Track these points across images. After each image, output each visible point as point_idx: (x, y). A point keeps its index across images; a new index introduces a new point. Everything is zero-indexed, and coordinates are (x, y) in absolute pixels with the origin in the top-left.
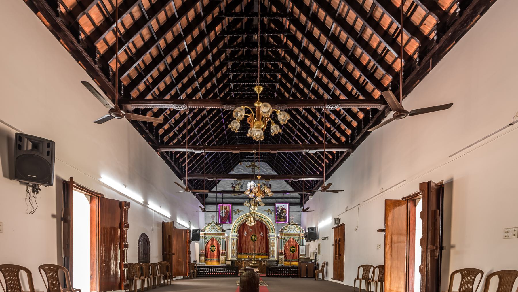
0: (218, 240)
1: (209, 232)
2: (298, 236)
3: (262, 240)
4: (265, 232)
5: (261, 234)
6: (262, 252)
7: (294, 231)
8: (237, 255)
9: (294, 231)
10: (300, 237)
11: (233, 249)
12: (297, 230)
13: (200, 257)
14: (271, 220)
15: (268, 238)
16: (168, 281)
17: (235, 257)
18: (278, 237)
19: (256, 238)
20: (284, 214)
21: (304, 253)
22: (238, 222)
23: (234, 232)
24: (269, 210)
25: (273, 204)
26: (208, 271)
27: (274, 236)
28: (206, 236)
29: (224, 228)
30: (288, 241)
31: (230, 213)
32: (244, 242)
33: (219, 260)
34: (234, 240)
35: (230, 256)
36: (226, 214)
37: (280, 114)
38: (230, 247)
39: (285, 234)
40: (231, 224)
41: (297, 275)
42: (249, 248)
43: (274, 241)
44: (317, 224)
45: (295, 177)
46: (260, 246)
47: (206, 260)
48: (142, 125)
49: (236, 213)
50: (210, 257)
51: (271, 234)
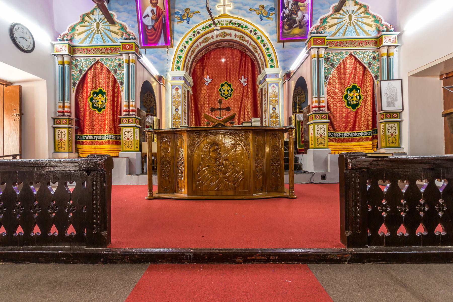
1: (86, 43)
3: (245, 94)
5: (242, 80)
11: (177, 113)
12: (366, 28)
14: (267, 35)
19: (232, 90)
20: (300, 13)
22: (187, 42)
24: (263, 7)
27: (276, 75)
30: (339, 69)
32: (204, 101)
46: (240, 109)
51: (268, 71)
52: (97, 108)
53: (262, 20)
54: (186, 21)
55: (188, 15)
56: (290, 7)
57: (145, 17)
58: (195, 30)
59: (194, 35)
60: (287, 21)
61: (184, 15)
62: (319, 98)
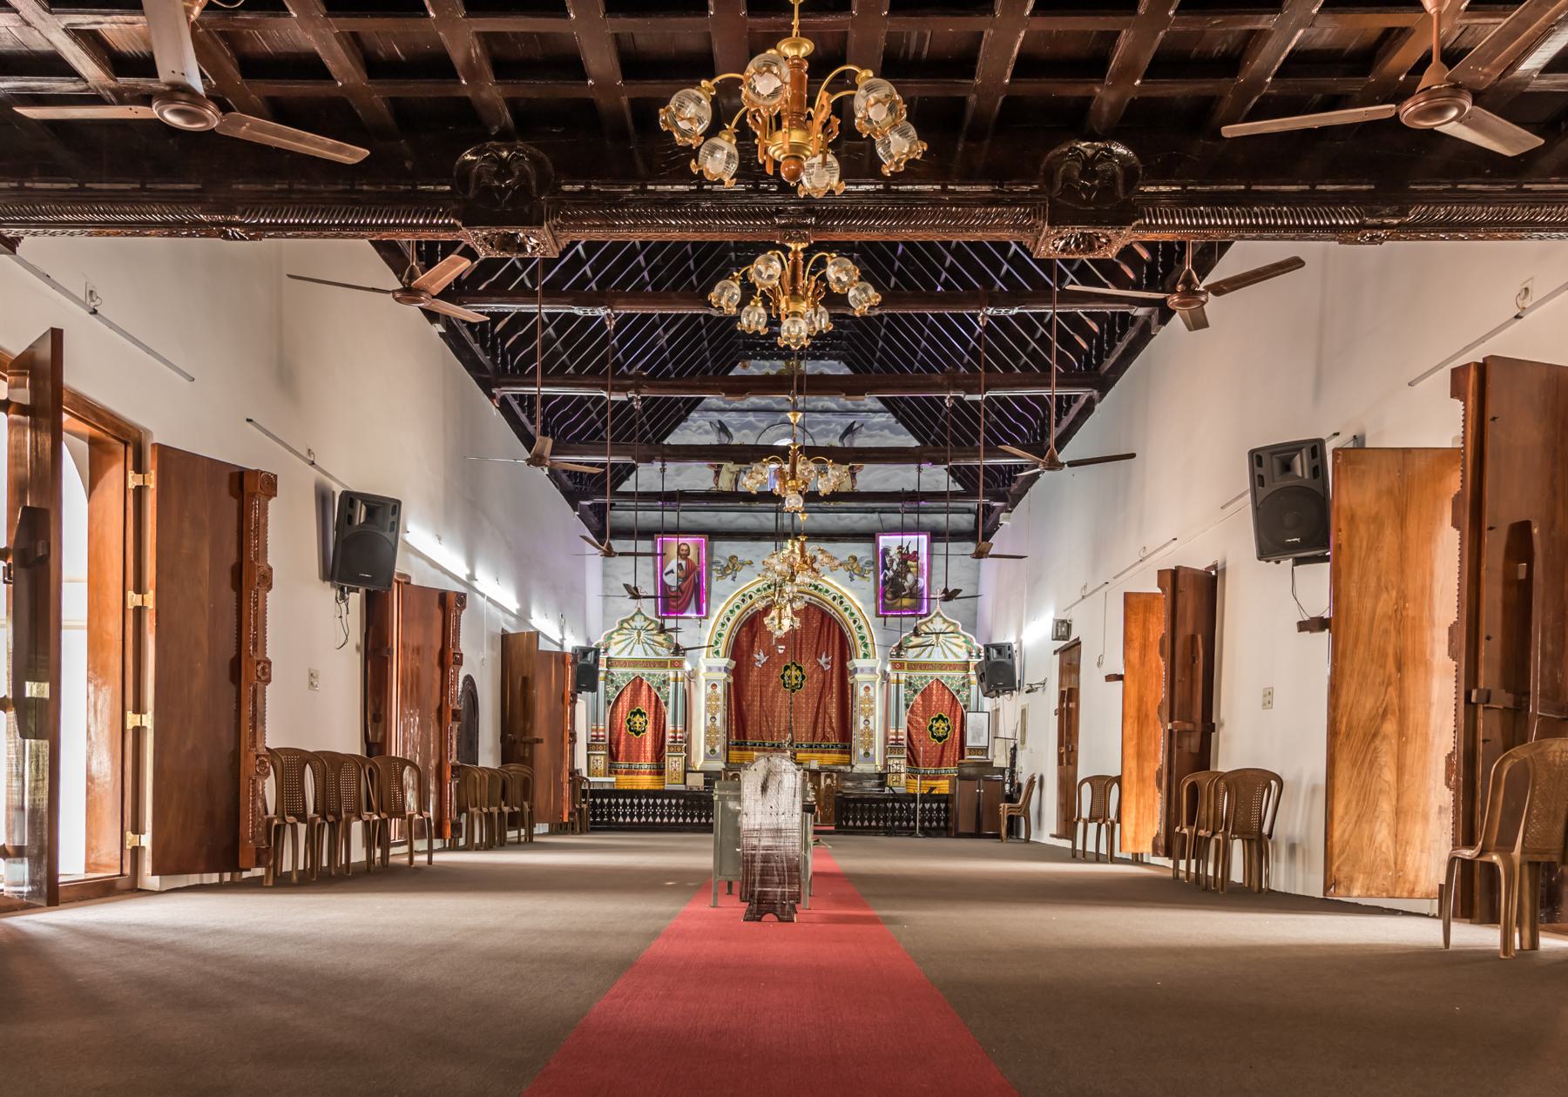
0: (659, 689)
1: (624, 655)
2: (959, 674)
3: (827, 685)
4: (837, 653)
6: (824, 737)
7: (947, 651)
8: (727, 749)
9: (947, 651)
10: (968, 676)
11: (713, 724)
12: (955, 648)
13: (588, 756)
15: (850, 680)
16: (519, 833)
17: (717, 758)
18: (885, 675)
19: (803, 677)
20: (910, 577)
21: (983, 743)
22: (732, 612)
23: (717, 652)
24: (855, 559)
25: (869, 536)
26: (628, 811)
27: (872, 670)
28: (612, 670)
29: (683, 640)
30: (923, 693)
31: (700, 575)
32: (753, 696)
33: (659, 771)
34: (714, 686)
35: (699, 751)
36: (685, 579)
37: (833, 468)
38: (699, 718)
39: (913, 666)
40: (706, 618)
41: (946, 828)
42: (773, 722)
43: (871, 693)
44: (1020, 631)
45: (935, 455)
46: (817, 712)
47: (612, 770)
48: (466, 334)
49: (724, 573)
50: (628, 758)
52: (634, 731)
53: (852, 580)
54: (730, 577)
55: (734, 566)
56: (895, 567)
57: (666, 574)
58: (746, 592)
59: (743, 601)
60: (891, 587)
61: (728, 566)
62: (897, 729)
